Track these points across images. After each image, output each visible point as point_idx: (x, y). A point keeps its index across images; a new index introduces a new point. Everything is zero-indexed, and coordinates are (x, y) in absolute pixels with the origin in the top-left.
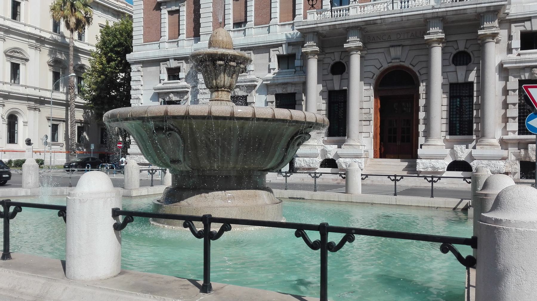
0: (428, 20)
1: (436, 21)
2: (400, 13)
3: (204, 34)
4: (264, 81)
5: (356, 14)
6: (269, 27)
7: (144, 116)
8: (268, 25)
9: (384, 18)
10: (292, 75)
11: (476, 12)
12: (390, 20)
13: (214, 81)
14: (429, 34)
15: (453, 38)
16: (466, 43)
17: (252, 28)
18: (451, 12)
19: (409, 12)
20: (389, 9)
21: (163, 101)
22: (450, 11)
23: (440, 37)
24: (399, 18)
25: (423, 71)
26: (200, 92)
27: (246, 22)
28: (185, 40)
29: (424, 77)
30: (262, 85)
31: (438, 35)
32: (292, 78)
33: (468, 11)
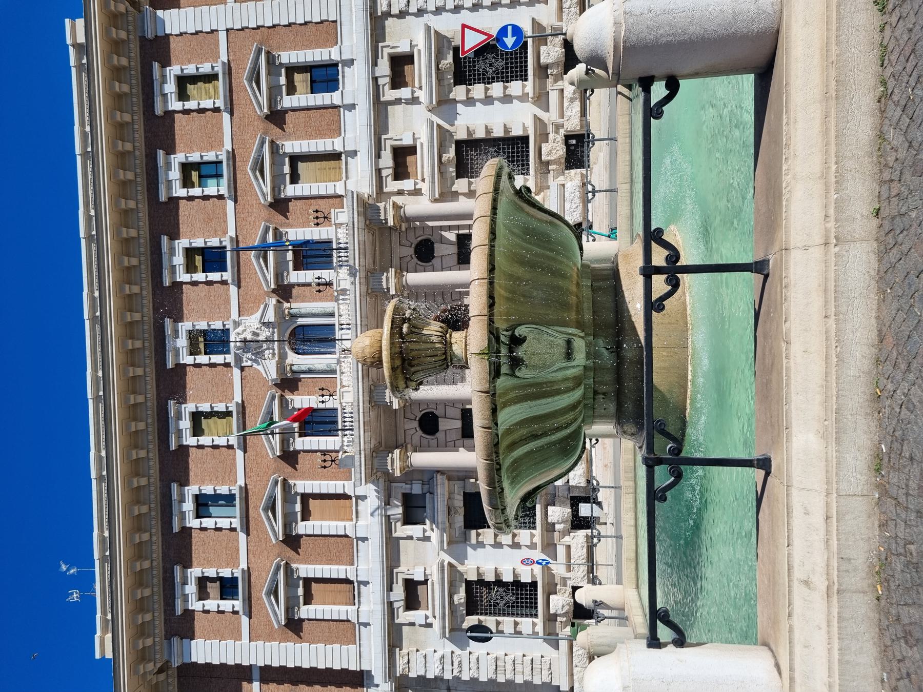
4: (444, 636)
5: (352, 393)
6: (360, 624)
8: (355, 540)
10: (435, 497)
15: (396, 261)
23: (393, 273)
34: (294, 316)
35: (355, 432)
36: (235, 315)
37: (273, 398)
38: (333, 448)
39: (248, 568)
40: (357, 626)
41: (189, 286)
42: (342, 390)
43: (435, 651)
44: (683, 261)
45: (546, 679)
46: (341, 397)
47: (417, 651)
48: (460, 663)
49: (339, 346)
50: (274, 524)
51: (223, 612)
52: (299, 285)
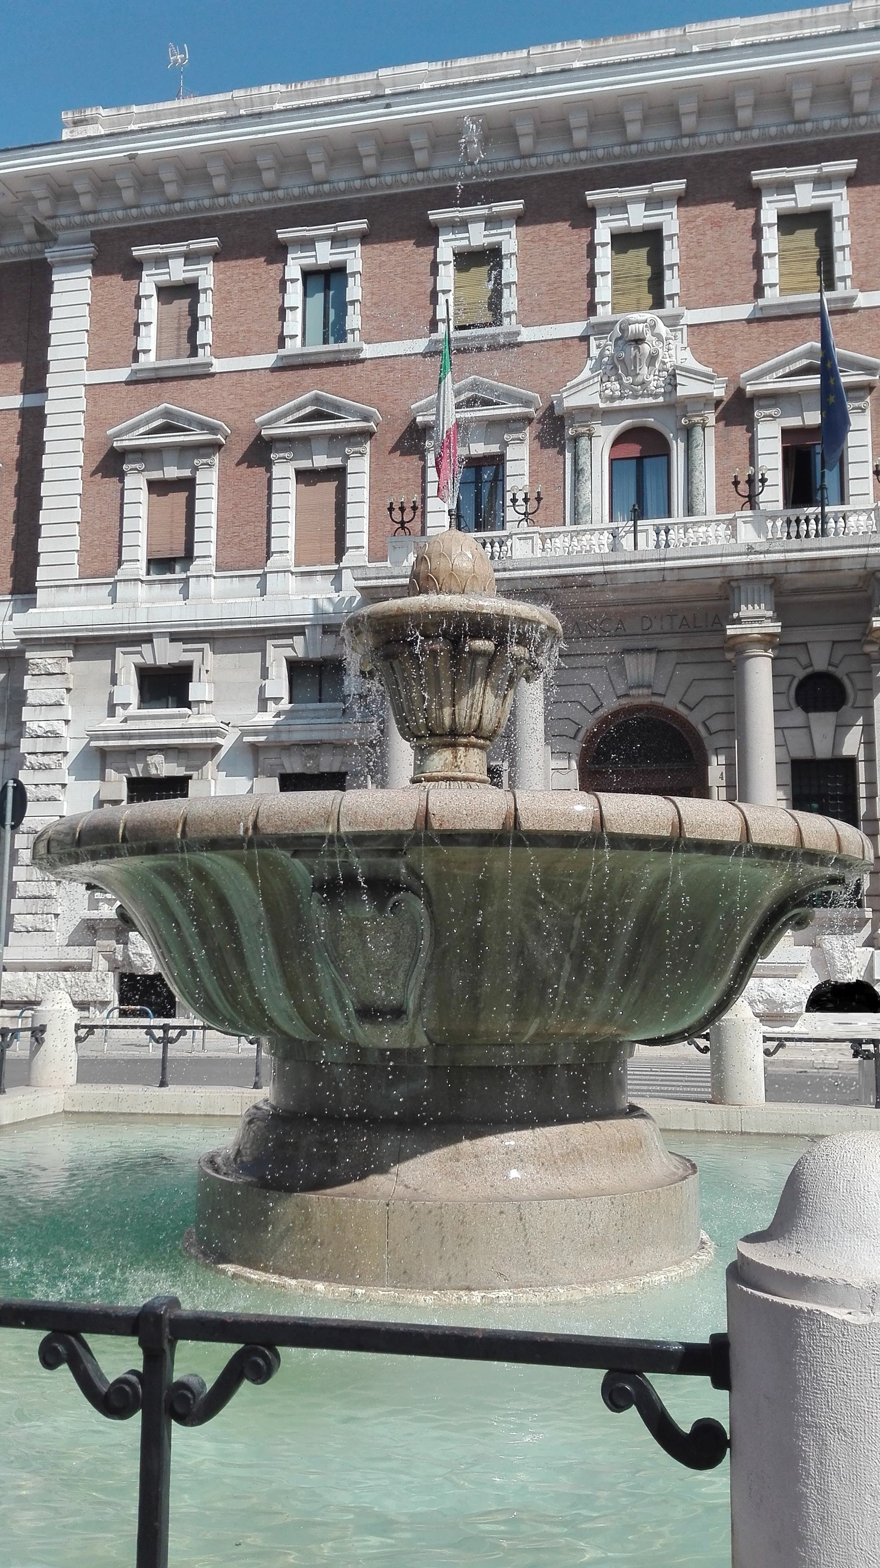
0: (733, 584)
1: (756, 587)
2: (660, 560)
3: (52, 587)
4: (244, 733)
5: (530, 555)
6: (265, 575)
7: (320, 830)
8: (260, 572)
9: (615, 572)
11: (865, 568)
12: (631, 579)
13: (447, 711)
14: (739, 621)
15: (797, 636)
16: (832, 649)
17: (210, 576)
18: (798, 564)
19: (684, 558)
20: (625, 548)
21: (13, 787)
22: (796, 561)
23: (770, 630)
24: (655, 573)
25: (716, 724)
26: (28, 764)
27: (188, 557)
28: (215, 578)
29: (720, 741)
30: (238, 745)
31: (763, 625)
32: (335, 729)
33: (845, 565)
34: (688, 432)
35: (794, 543)
36: (693, 317)
37: (527, 403)
38: (429, 523)
39: (213, 375)
40: (111, 580)
41: (752, 221)
42: (536, 536)
43: (67, 722)
44: (178, 1433)
45: (20, 922)
46: (525, 537)
47: (69, 690)
48: (47, 768)
49: (624, 525)
50: (290, 419)
51: (137, 333)
52: (752, 442)
